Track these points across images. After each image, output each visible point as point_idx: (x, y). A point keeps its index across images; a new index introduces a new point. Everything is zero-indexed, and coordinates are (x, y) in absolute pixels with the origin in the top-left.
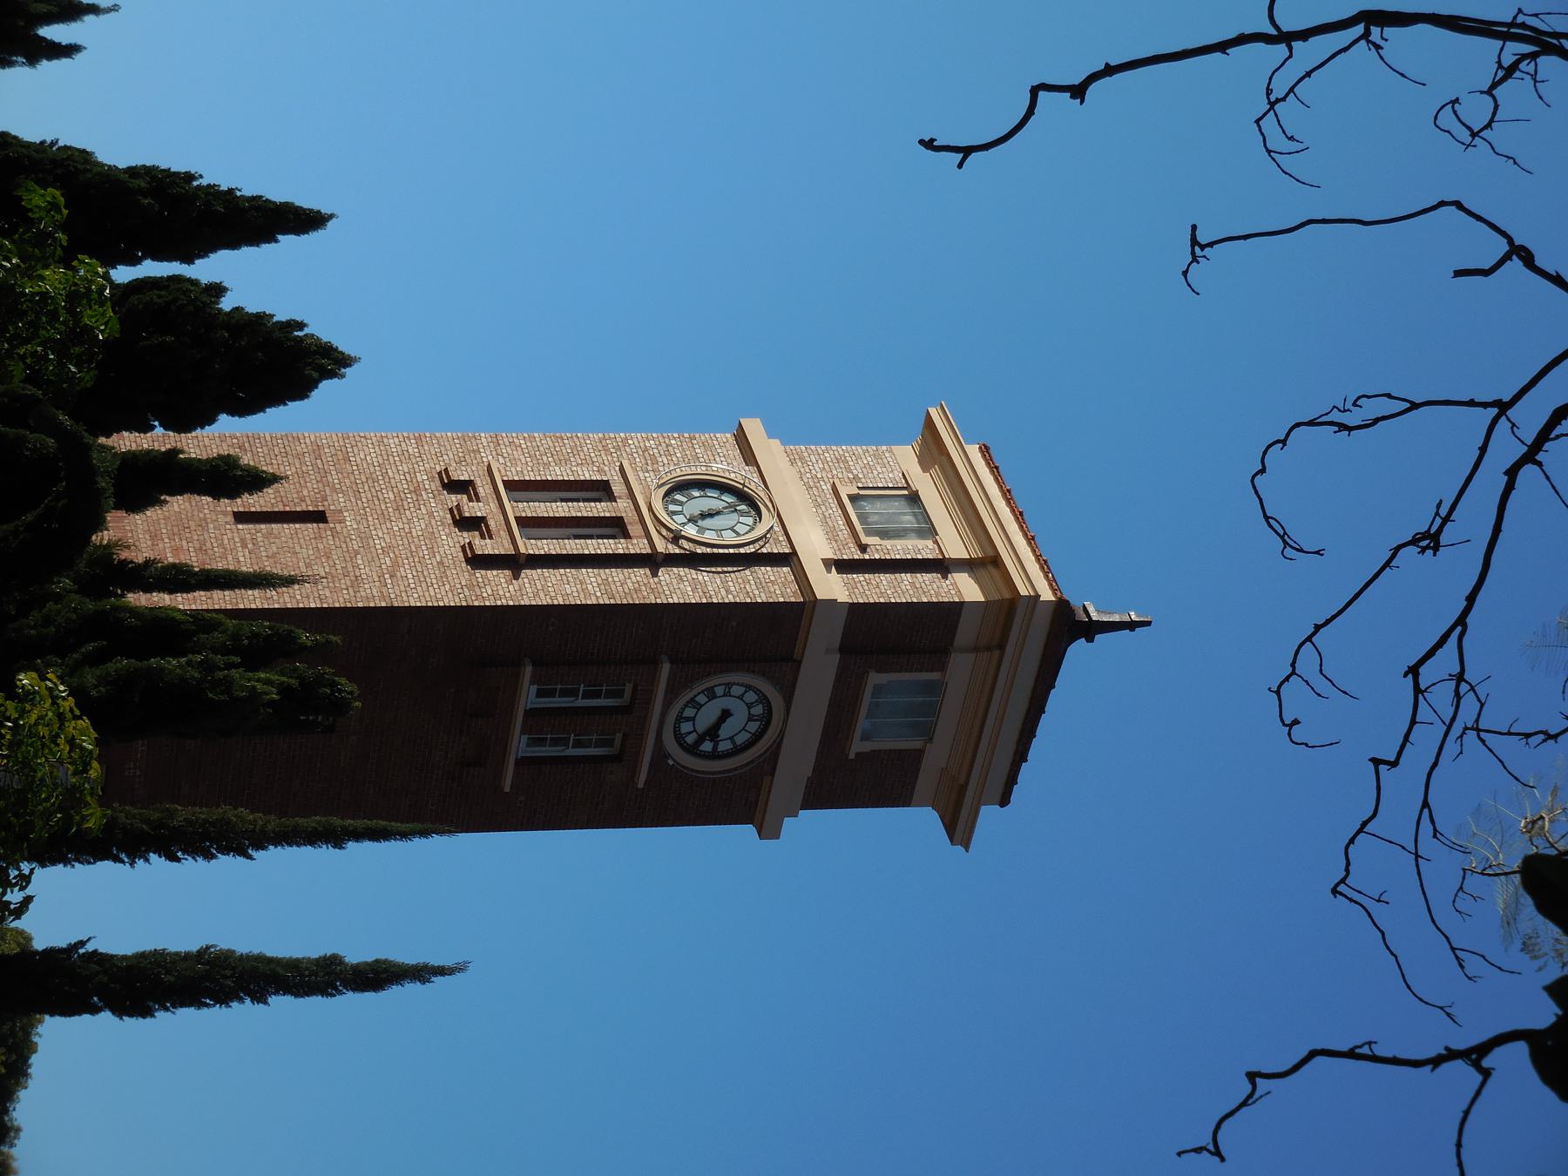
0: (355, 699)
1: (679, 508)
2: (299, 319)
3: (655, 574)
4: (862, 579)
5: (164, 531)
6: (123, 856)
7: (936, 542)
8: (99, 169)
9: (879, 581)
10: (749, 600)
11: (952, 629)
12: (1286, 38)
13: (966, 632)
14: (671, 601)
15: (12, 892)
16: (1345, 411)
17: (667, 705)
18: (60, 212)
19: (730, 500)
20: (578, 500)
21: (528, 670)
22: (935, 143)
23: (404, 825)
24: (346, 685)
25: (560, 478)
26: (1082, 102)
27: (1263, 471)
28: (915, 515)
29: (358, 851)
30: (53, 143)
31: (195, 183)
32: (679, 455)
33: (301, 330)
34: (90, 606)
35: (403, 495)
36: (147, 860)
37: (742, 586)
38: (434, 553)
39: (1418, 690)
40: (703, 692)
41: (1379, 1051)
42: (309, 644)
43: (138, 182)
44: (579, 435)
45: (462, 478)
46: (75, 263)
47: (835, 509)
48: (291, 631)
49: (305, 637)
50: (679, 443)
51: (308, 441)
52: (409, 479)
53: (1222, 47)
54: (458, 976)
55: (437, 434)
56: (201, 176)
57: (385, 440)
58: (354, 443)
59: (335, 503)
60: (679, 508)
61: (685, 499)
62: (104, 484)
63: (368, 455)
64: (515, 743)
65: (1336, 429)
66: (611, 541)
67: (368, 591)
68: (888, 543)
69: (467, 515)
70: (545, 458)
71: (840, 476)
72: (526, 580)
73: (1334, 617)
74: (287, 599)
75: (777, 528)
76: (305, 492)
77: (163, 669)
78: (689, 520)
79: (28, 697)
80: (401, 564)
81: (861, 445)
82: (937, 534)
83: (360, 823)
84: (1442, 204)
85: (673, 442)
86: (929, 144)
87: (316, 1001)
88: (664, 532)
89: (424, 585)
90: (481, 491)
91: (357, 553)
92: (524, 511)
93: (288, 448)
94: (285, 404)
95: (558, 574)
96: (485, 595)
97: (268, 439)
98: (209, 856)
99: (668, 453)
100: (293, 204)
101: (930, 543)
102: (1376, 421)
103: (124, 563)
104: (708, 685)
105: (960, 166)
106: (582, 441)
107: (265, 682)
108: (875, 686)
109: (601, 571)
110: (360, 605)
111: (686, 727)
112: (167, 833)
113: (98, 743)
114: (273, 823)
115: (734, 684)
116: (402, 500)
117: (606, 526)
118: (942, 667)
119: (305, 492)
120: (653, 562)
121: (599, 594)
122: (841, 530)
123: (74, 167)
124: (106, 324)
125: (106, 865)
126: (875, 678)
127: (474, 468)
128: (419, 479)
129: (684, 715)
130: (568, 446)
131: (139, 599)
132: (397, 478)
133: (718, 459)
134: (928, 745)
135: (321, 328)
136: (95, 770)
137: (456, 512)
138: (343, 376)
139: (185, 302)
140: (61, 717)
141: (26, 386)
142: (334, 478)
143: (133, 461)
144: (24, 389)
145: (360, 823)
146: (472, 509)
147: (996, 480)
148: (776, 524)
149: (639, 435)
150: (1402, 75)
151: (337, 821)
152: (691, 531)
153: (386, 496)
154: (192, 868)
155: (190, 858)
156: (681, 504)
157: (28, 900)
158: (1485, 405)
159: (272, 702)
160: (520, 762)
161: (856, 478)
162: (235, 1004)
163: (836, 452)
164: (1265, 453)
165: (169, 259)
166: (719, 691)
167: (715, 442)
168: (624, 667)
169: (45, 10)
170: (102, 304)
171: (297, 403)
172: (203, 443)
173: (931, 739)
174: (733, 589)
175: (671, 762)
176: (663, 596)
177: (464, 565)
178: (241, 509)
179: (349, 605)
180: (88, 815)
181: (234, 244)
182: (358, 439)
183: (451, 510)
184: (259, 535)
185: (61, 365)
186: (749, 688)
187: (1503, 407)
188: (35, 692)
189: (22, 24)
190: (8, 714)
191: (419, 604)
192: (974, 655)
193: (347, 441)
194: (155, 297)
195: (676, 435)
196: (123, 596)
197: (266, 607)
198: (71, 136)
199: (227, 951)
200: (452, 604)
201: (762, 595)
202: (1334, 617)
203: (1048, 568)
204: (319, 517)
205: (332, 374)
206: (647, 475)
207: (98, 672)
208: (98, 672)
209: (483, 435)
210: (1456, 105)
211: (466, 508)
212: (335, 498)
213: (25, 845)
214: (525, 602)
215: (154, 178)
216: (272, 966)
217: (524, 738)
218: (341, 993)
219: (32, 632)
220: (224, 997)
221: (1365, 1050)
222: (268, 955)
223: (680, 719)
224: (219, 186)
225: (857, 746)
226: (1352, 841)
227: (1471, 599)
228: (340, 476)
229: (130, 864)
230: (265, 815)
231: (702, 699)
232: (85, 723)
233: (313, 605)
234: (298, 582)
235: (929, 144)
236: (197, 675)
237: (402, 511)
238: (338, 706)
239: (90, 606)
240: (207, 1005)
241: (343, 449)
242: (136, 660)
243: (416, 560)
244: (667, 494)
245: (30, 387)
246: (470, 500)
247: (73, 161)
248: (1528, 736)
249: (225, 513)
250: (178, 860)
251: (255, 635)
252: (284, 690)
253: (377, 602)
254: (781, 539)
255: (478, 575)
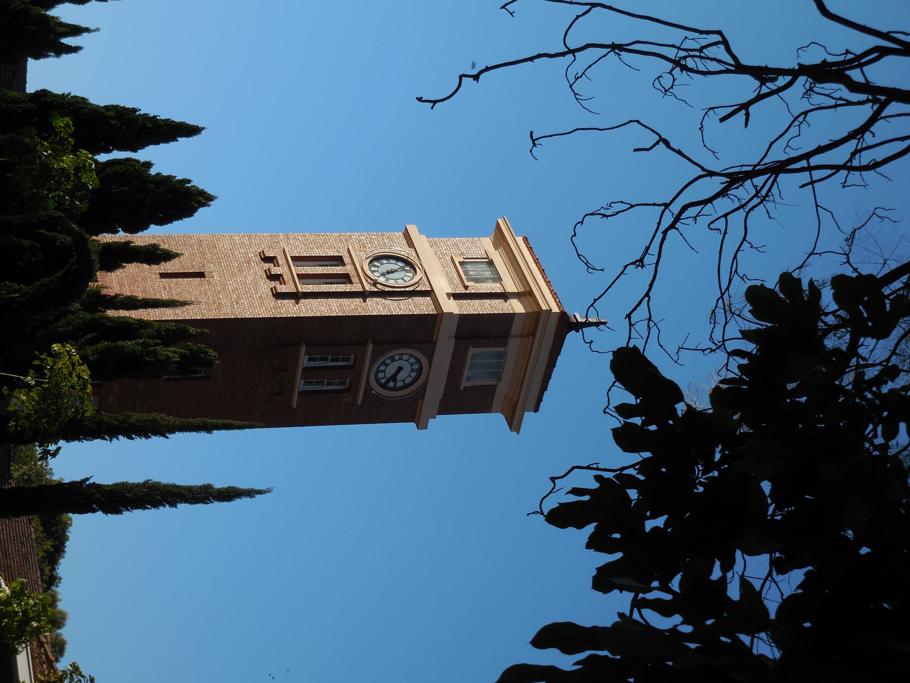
0: (217, 359)
1: (376, 269)
2: (188, 178)
3: (365, 301)
4: (466, 302)
5: (126, 282)
6: (106, 437)
7: (502, 284)
8: (91, 107)
9: (474, 303)
10: (410, 313)
11: (510, 326)
12: (573, 52)
13: (516, 328)
14: (372, 314)
15: (51, 445)
16: (607, 209)
17: (372, 364)
18: (70, 129)
19: (401, 265)
20: (327, 266)
21: (304, 349)
22: (423, 99)
23: (240, 422)
24: (212, 353)
25: (318, 255)
26: (477, 82)
27: (575, 235)
28: (491, 271)
29: (219, 435)
30: (68, 95)
31: (137, 113)
32: (376, 243)
33: (189, 183)
34: (89, 316)
35: (242, 264)
36: (118, 439)
37: (407, 307)
38: (257, 292)
39: (631, 325)
40: (389, 358)
41: (600, 466)
42: (194, 333)
43: (109, 113)
44: (328, 234)
45: (271, 255)
46: (78, 153)
47: (452, 269)
48: (186, 327)
49: (192, 330)
50: (376, 238)
51: (195, 238)
52: (245, 256)
53: (531, 59)
54: (268, 494)
55: (258, 234)
56: (140, 110)
57: (233, 237)
58: (218, 239)
59: (208, 268)
60: (376, 269)
61: (379, 265)
62: (94, 257)
63: (224, 245)
64: (298, 384)
65: (602, 216)
66: (343, 285)
67: (226, 311)
68: (478, 285)
69: (273, 273)
70: (311, 245)
71: (455, 252)
72: (302, 305)
73: (602, 296)
74: (186, 315)
75: (424, 278)
76: (194, 263)
77: (124, 346)
78: (381, 275)
79: (56, 356)
80: (241, 298)
81: (465, 237)
82: (502, 281)
83: (219, 422)
84: (631, 121)
85: (373, 237)
86: (420, 99)
87: (200, 506)
88: (369, 281)
89: (252, 307)
90: (280, 261)
91: (220, 292)
92: (301, 271)
93: (186, 242)
94: (182, 219)
95: (317, 302)
96: (282, 312)
97: (176, 237)
98: (147, 437)
99: (371, 242)
100: (185, 122)
101: (498, 285)
102: (618, 213)
103: (105, 296)
104: (390, 355)
105: (432, 108)
106: (329, 237)
107: (173, 352)
108: (473, 354)
109: (339, 300)
110: (222, 317)
111: (381, 375)
112: (127, 426)
113: (91, 376)
114: (178, 421)
115: (404, 354)
116: (241, 266)
117: (341, 278)
118: (505, 345)
119: (194, 263)
120: (364, 295)
121: (337, 311)
122: (455, 279)
123: (79, 106)
124: (93, 181)
125: (99, 441)
126: (472, 351)
127: (276, 251)
128: (250, 256)
129: (380, 369)
130: (322, 239)
131: (111, 313)
132: (239, 255)
133: (395, 245)
134: (499, 383)
135: (199, 182)
136: (89, 389)
137: (268, 272)
138: (210, 205)
139: (133, 171)
140: (73, 364)
141: (57, 212)
142: (208, 256)
143: (108, 247)
144: (56, 213)
145: (219, 422)
146: (275, 270)
147: (531, 254)
148: (423, 276)
149: (357, 234)
150: (630, 66)
151: (208, 420)
152: (382, 280)
153: (234, 264)
154: (139, 442)
155: (138, 438)
156: (378, 267)
157: (59, 449)
158: (659, 205)
159: (176, 362)
160: (300, 393)
161: (463, 253)
162: (161, 508)
163: (453, 241)
164: (575, 227)
165: (126, 150)
166: (397, 357)
167: (394, 237)
168: (353, 346)
169: (64, 31)
170: (91, 171)
171: (188, 219)
172: (142, 238)
173: (500, 380)
174: (403, 308)
175: (374, 392)
176: (368, 311)
177: (272, 297)
178: (163, 272)
179: (216, 317)
180: (86, 410)
181: (157, 143)
182: (220, 237)
183: (265, 271)
184: (172, 284)
185: (72, 201)
186: (411, 356)
187: (666, 206)
188: (61, 353)
189: (53, 37)
190: (48, 363)
191: (250, 317)
192: (521, 339)
193: (214, 238)
194: (119, 168)
195: (375, 233)
196: (105, 312)
197: (176, 319)
198: (77, 91)
200: (267, 316)
201: (417, 311)
202: (602, 296)
203: (557, 296)
204: (201, 275)
205: (204, 205)
206: (361, 253)
207: (93, 348)
208: (93, 348)
209: (281, 234)
210: (660, 78)
211: (272, 270)
212: (209, 265)
213: (57, 423)
214: (302, 315)
215: (117, 111)
216: (179, 489)
217: (302, 381)
218: (212, 502)
219: (61, 329)
220: (156, 504)
221: (595, 466)
222: (177, 484)
223: (378, 371)
224: (149, 114)
225: (464, 384)
226: (610, 390)
227: (651, 286)
228: (211, 255)
229: (110, 441)
230: (174, 417)
231: (388, 361)
232: (85, 367)
233: (198, 318)
234: (189, 304)
235: (420, 99)
236: (140, 349)
237: (242, 272)
238: (209, 363)
239: (89, 316)
240: (148, 508)
241: (213, 242)
242: (111, 342)
243: (249, 295)
244: (371, 262)
245: (59, 212)
246: (275, 266)
247: (78, 103)
248: (704, 350)
249: (155, 274)
250: (133, 439)
251: (168, 330)
252: (182, 356)
253: (230, 316)
254: (426, 283)
255: (279, 302)
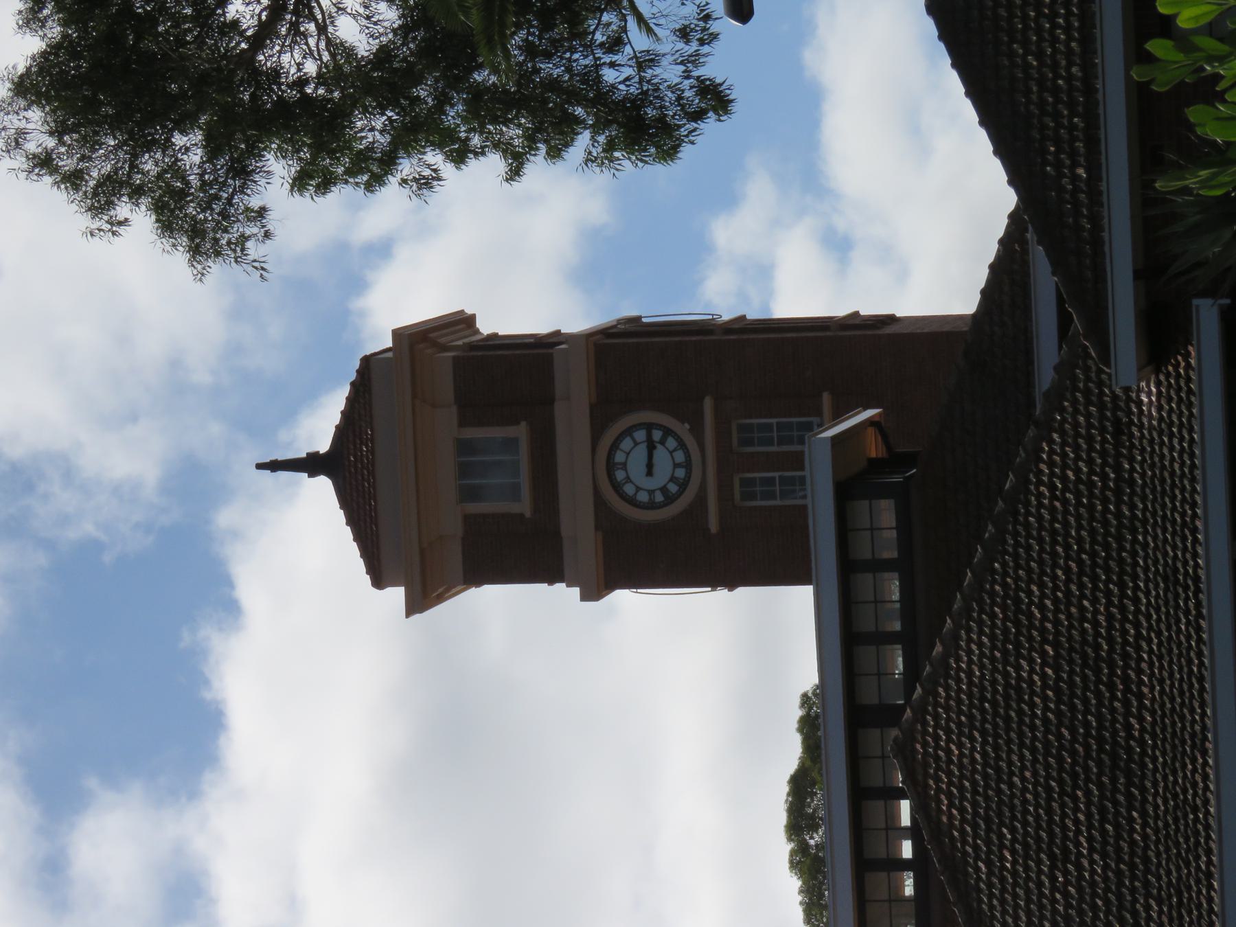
13: (454, 556)
118: (468, 519)
199: (573, 140)
